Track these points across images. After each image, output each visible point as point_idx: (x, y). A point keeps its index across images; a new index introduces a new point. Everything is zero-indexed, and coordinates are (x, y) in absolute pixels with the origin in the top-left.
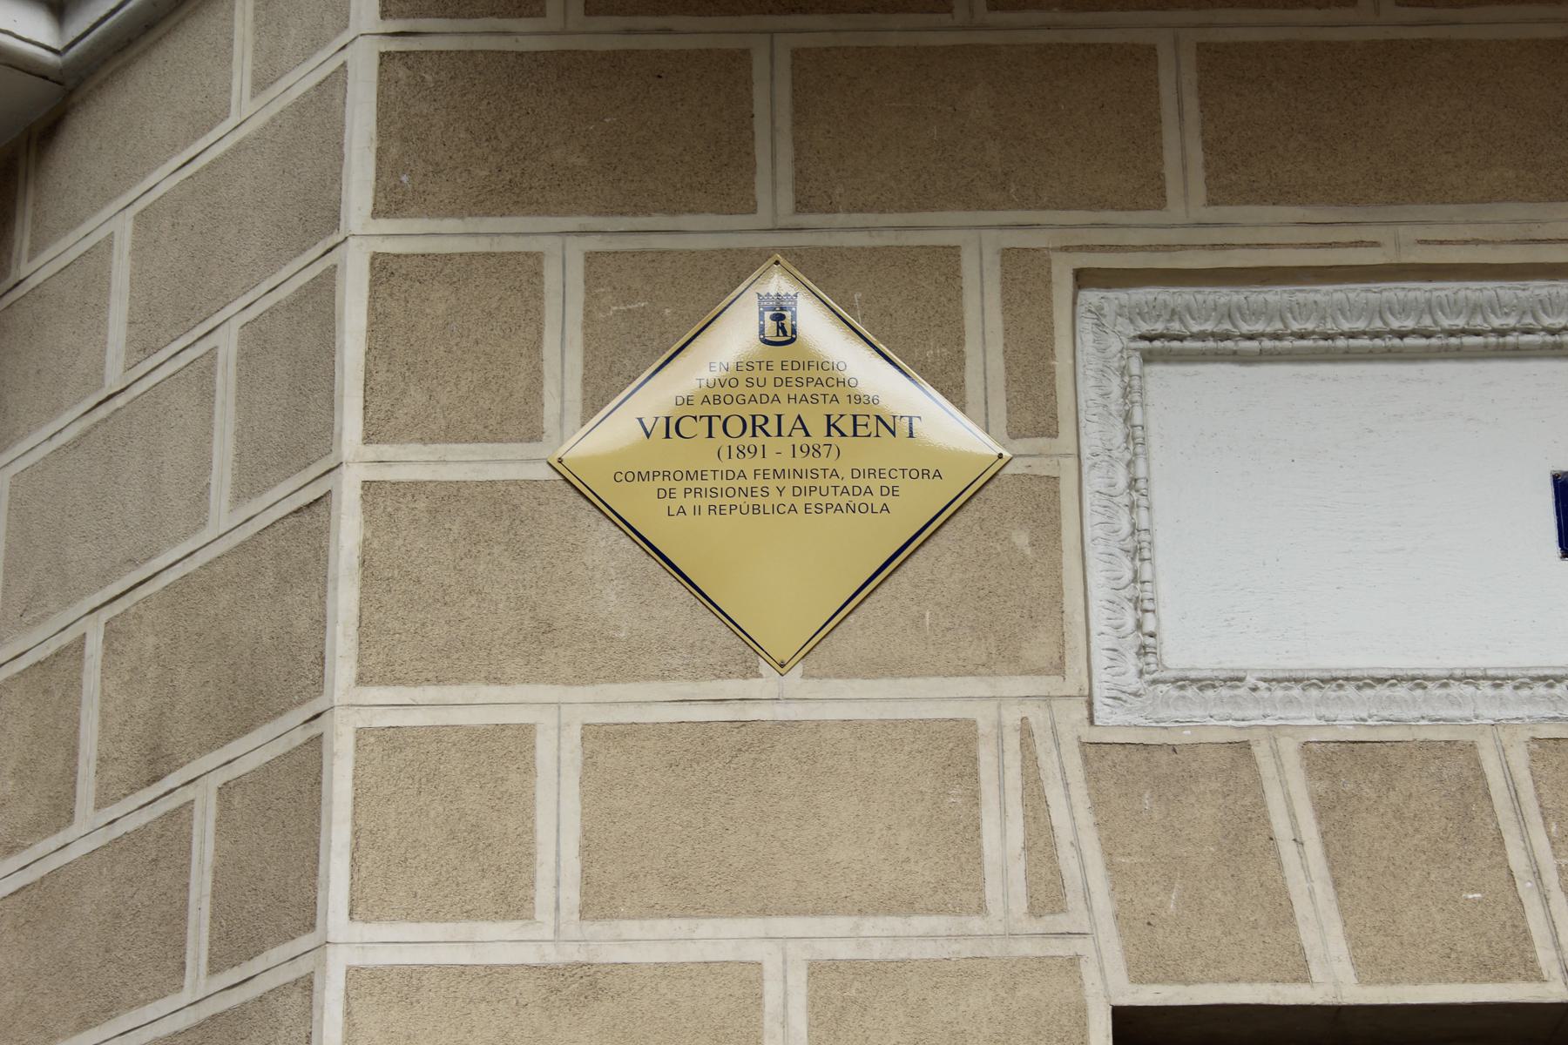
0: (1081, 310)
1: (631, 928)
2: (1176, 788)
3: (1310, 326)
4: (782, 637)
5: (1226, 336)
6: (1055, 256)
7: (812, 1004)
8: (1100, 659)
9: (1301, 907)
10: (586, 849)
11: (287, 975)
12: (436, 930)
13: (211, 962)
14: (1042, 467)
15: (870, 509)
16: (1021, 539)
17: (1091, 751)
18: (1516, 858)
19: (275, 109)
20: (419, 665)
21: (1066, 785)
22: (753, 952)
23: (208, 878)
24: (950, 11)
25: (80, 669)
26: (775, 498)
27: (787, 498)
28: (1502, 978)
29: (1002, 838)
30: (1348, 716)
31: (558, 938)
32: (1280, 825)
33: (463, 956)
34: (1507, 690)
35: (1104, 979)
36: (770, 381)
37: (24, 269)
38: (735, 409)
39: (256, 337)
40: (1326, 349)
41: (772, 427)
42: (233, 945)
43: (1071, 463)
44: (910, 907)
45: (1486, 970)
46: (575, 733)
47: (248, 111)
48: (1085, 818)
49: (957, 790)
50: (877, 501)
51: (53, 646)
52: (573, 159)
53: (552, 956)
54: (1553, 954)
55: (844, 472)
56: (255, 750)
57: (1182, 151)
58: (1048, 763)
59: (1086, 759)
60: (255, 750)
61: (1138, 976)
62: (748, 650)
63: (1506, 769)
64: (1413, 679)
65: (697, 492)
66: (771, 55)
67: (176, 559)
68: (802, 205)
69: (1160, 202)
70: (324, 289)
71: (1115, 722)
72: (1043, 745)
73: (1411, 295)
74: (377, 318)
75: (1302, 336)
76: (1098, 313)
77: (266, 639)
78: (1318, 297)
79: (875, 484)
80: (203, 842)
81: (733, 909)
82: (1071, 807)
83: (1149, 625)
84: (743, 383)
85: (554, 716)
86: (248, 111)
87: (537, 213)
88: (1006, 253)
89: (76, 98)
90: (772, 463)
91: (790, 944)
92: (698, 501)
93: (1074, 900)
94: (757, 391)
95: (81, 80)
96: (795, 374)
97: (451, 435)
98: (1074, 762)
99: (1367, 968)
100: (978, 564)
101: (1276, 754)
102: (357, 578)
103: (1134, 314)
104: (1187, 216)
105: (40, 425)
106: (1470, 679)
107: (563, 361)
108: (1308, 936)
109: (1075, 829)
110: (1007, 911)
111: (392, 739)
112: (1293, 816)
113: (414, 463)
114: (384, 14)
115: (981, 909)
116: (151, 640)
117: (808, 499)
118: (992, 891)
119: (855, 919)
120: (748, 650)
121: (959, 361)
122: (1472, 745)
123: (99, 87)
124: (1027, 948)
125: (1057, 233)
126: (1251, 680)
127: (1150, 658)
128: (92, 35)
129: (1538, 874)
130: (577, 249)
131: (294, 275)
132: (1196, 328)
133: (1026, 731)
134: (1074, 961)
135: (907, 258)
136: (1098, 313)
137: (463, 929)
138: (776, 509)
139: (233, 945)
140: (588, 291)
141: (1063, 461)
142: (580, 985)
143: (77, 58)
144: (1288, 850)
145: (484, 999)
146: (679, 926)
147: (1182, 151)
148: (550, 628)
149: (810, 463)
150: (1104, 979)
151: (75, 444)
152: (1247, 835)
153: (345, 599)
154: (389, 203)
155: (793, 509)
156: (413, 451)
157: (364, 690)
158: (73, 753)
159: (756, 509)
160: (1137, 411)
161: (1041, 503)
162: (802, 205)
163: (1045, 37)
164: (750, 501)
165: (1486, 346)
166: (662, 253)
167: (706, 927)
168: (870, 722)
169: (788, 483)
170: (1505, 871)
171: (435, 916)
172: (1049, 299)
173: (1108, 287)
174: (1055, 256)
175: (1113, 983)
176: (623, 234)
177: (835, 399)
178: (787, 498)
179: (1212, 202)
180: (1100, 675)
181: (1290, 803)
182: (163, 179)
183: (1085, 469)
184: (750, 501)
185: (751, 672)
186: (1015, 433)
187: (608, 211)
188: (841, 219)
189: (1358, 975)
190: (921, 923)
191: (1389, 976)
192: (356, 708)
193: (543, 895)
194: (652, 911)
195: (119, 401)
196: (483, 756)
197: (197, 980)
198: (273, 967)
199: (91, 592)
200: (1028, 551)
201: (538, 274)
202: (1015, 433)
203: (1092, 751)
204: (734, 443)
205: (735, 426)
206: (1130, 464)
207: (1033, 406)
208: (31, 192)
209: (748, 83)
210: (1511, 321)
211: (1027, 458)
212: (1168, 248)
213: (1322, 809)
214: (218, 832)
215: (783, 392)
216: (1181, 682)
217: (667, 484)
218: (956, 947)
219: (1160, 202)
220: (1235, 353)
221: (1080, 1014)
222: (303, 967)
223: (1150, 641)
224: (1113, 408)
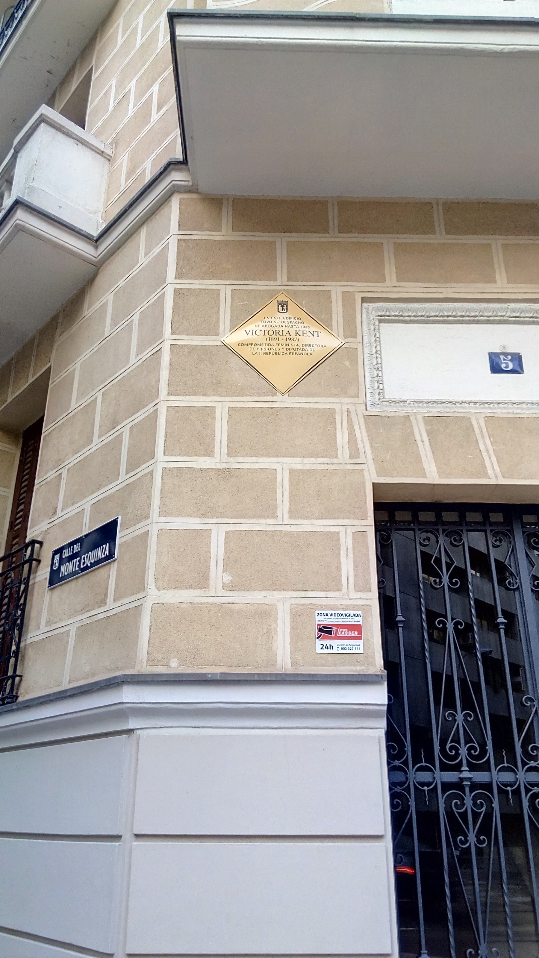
0: (363, 308)
1: (241, 459)
2: (389, 426)
3: (423, 314)
4: (282, 384)
5: (402, 316)
6: (356, 294)
7: (290, 480)
8: (368, 395)
9: (423, 458)
11: (147, 471)
13: (126, 471)
14: (353, 346)
15: (307, 354)
16: (347, 363)
17: (366, 417)
18: (482, 447)
19: (150, 259)
20: (184, 391)
21: (360, 425)
22: (273, 466)
23: (126, 450)
24: (329, 233)
25: (96, 405)
26: (281, 351)
27: (285, 351)
28: (479, 478)
29: (342, 439)
30: (435, 411)
31: (220, 462)
32: (418, 437)
33: (194, 465)
34: (477, 405)
35: (370, 475)
36: (280, 322)
37: (86, 313)
38: (271, 328)
39: (143, 316)
41: (281, 333)
42: (132, 466)
43: (361, 344)
44: (317, 456)
46: (226, 409)
47: (143, 260)
48: (365, 434)
49: (330, 426)
50: (309, 353)
51: (89, 401)
52: (228, 267)
53: (219, 466)
54: (492, 471)
55: (300, 344)
56: (140, 416)
58: (355, 420)
59: (365, 418)
60: (140, 416)
61: (379, 475)
62: (273, 390)
63: (479, 425)
64: (452, 402)
65: (261, 349)
66: (282, 241)
67: (120, 373)
69: (384, 281)
70: (162, 298)
71: (372, 411)
72: (353, 415)
73: (450, 306)
74: (175, 304)
75: (422, 316)
76: (368, 309)
77: (143, 388)
78: (425, 306)
79: (308, 348)
80: (125, 442)
82: (361, 431)
83: (381, 387)
84: (273, 322)
85: (221, 405)
86: (143, 260)
87: (219, 279)
88: (343, 292)
89: (100, 270)
90: (281, 342)
91: (284, 465)
92: (261, 351)
93: (362, 455)
94: (277, 324)
95: (102, 265)
96: (287, 320)
98: (362, 420)
99: (441, 474)
100: (334, 371)
101: (416, 419)
102: (168, 368)
103: (378, 309)
105: (88, 349)
106: (469, 403)
107: (225, 317)
108: (426, 466)
109: (362, 437)
110: (344, 457)
111: (177, 409)
112: (421, 435)
113: (185, 340)
114: (179, 229)
115: (337, 457)
116: (114, 394)
117: (290, 351)
118: (339, 452)
119: (302, 459)
120: (273, 390)
121: (331, 319)
122: (469, 418)
123: (106, 266)
124: (349, 467)
125: (359, 288)
126: (408, 402)
127: (382, 395)
129: (488, 451)
130: (229, 288)
131: (154, 297)
132: (393, 314)
133: (348, 411)
134: (362, 470)
137: (195, 458)
138: (282, 353)
139: (132, 466)
140: (232, 299)
141: (359, 344)
142: (227, 474)
143: (101, 259)
144: (420, 444)
145: (200, 477)
146: (254, 459)
148: (220, 383)
149: (291, 342)
150: (370, 475)
151: (97, 351)
152: (409, 438)
153: (164, 374)
154: (179, 275)
155: (286, 354)
157: (170, 397)
158: (93, 427)
159: (276, 353)
160: (378, 334)
161: (352, 354)
162: (289, 280)
163: (353, 240)
164: (275, 351)
165: (470, 320)
166: (252, 290)
167: (261, 460)
168: (306, 408)
169: (285, 347)
170: (479, 450)
172: (355, 304)
173: (370, 302)
174: (356, 294)
175: (372, 476)
176: (241, 285)
177: (298, 327)
178: (285, 351)
179: (397, 281)
180: (368, 399)
181: (420, 432)
182: (121, 283)
183: (364, 347)
184: (275, 351)
186: (345, 337)
188: (300, 283)
189: (439, 476)
190: (320, 460)
191: (448, 477)
192: (166, 401)
193: (217, 450)
195: (108, 339)
196: (201, 414)
197: (123, 476)
198: (143, 470)
199: (100, 386)
200: (349, 367)
201: (219, 294)
202: (345, 337)
203: (367, 417)
204: (271, 337)
205: (271, 333)
206: (376, 347)
207: (350, 330)
208: (88, 294)
209: (275, 249)
210: (477, 314)
211: (351, 343)
213: (429, 433)
214: (129, 438)
215: (284, 325)
216: (391, 401)
217: (252, 347)
218: (329, 466)
219: (384, 281)
220: (403, 321)
221: (364, 484)
222: (150, 468)
223: (381, 391)
224: (372, 333)
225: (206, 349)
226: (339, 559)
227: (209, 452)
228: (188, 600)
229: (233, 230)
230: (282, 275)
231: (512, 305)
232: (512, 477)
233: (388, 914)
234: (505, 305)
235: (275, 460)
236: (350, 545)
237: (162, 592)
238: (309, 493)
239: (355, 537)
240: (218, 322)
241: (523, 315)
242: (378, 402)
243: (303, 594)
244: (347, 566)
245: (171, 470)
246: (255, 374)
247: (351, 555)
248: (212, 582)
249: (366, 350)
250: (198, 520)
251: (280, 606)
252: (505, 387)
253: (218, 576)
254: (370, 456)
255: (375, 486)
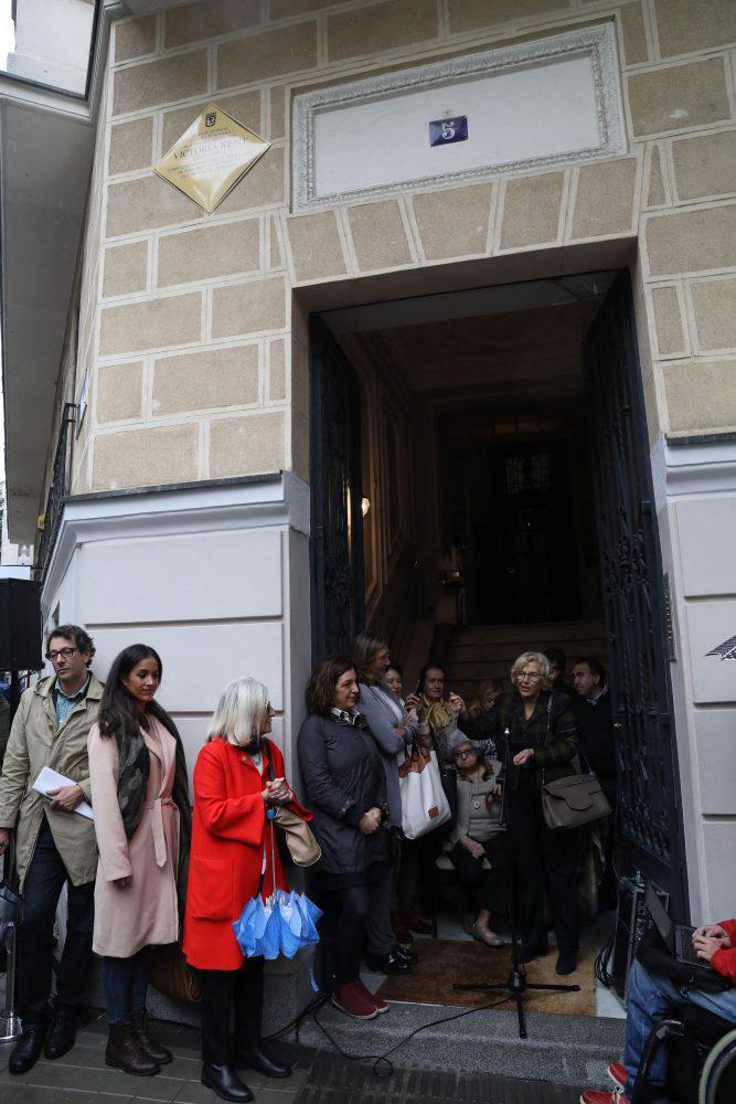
4: (208, 201)
10: (160, 270)
12: (123, 297)
16: (273, 167)
18: (407, 230)
29: (265, 248)
40: (365, 100)
45: (397, 262)
57: (322, 49)
61: (300, 278)
62: (200, 210)
63: (406, 202)
68: (219, 88)
81: (195, 279)
85: (152, 237)
93: (283, 262)
97: (131, 168)
99: (361, 268)
104: (324, 67)
108: (346, 261)
120: (200, 210)
121: (259, 122)
124: (269, 276)
125: (286, 81)
128: (208, 528)
135: (245, 96)
136: (300, 105)
144: (342, 239)
147: (322, 49)
154: (116, 112)
156: (121, 175)
162: (219, 88)
171: (123, 293)
175: (293, 281)
176: (172, 106)
185: (201, 216)
187: (171, 101)
188: (230, 89)
193: (148, 284)
194: (176, 283)
201: (152, 122)
212: (299, 81)
225: (141, 183)
226: (257, 371)
227: (141, 287)
228: (125, 429)
229: (166, 47)
230: (212, 85)
231: (457, 60)
232: (436, 257)
233: (281, 679)
234: (448, 62)
235: (199, 282)
236: (268, 355)
237: (103, 425)
238: (234, 312)
239: (273, 349)
240: (150, 153)
241: (469, 69)
242: (306, 202)
243: (221, 409)
244: (264, 375)
245: (109, 310)
246: (185, 198)
247: (268, 365)
248: (143, 410)
249: (295, 148)
250: (132, 354)
251: (201, 424)
252: (454, 157)
253: (148, 402)
254: (291, 261)
255: (297, 292)
